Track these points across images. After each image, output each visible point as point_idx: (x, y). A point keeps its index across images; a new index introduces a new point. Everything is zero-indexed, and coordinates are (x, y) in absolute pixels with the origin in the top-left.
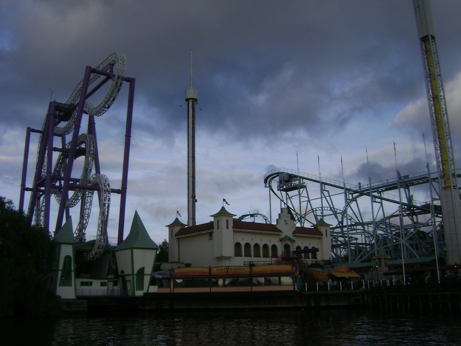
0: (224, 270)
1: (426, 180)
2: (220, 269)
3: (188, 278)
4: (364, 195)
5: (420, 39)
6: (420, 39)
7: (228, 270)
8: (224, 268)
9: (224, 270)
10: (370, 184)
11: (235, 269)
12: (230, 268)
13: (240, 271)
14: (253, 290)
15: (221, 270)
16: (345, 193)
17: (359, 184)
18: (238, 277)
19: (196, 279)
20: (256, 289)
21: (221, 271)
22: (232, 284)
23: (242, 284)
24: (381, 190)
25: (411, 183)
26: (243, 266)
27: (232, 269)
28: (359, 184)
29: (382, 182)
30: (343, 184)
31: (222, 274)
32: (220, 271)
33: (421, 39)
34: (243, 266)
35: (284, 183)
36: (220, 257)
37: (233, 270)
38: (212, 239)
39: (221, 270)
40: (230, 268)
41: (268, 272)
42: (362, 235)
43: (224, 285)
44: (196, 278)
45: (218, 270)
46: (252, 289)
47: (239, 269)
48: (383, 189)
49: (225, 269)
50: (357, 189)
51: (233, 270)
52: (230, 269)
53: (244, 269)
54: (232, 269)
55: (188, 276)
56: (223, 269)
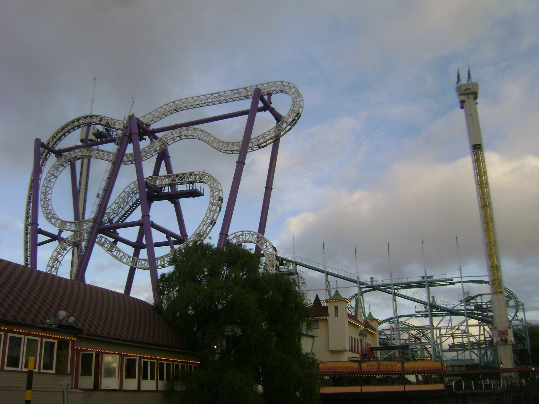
0: (375, 365)
1: (449, 282)
2: (370, 365)
3: (336, 375)
4: (378, 291)
5: (472, 145)
6: (472, 145)
7: (379, 366)
8: (375, 364)
9: (375, 365)
10: (392, 279)
11: (387, 365)
12: (382, 364)
13: (392, 367)
14: (363, 391)
15: (371, 366)
16: (358, 287)
17: (372, 278)
18: (430, 373)
19: (332, 376)
20: (408, 388)
21: (372, 366)
22: (426, 381)
23: (393, 382)
24: (396, 288)
25: (432, 284)
26: (347, 362)
27: (383, 365)
28: (372, 278)
29: (400, 279)
30: (356, 277)
31: (374, 371)
32: (371, 367)
33: (473, 146)
34: (348, 361)
35: (271, 271)
36: (342, 350)
37: (384, 365)
38: (319, 328)
39: (371, 366)
40: (382, 364)
41: (420, 369)
42: (427, 334)
43: (418, 382)
44: (346, 375)
45: (369, 366)
46: (405, 388)
47: (390, 365)
48: (399, 287)
49: (376, 364)
50: (369, 283)
51: (384, 365)
52: (382, 365)
53: (396, 366)
54: (383, 365)
55: (336, 372)
56: (374, 365)
